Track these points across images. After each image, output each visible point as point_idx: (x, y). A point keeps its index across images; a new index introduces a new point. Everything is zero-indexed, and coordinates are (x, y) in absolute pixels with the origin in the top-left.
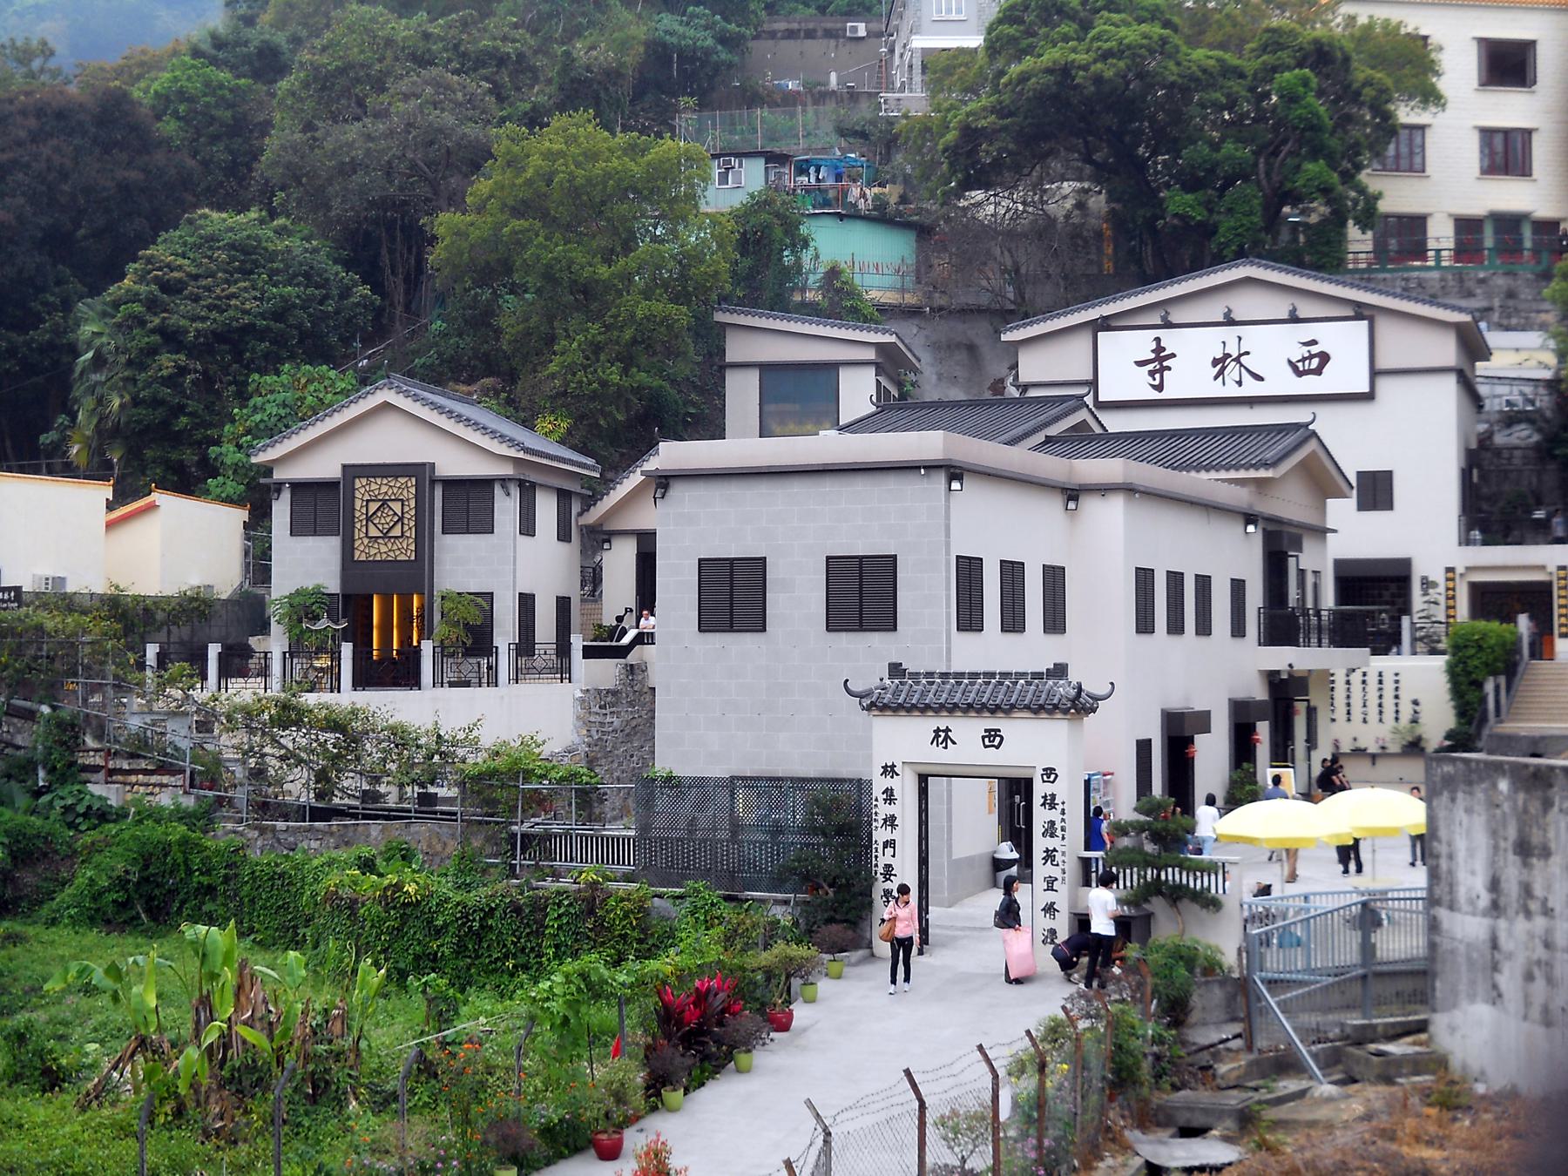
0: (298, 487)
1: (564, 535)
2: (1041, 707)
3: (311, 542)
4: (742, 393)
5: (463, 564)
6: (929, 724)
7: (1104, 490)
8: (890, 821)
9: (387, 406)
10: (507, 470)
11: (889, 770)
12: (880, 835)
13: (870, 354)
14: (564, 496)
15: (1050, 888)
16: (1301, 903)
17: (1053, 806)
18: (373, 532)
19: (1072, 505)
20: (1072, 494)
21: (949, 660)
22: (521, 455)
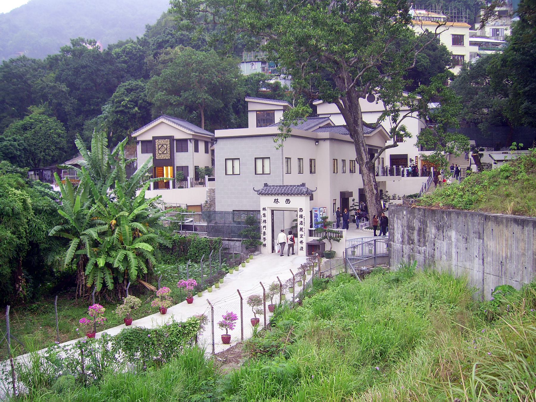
0: (143, 142)
1: (207, 151)
2: (292, 194)
3: (146, 155)
4: (252, 118)
5: (182, 159)
6: (273, 198)
7: (325, 139)
8: (265, 221)
9: (162, 122)
10: (191, 137)
11: (264, 209)
12: (262, 225)
13: (282, 108)
14: (206, 143)
15: (301, 237)
16: (361, 240)
17: (302, 217)
18: (160, 152)
19: (317, 144)
20: (317, 140)
21: (283, 181)
22: (194, 133)
